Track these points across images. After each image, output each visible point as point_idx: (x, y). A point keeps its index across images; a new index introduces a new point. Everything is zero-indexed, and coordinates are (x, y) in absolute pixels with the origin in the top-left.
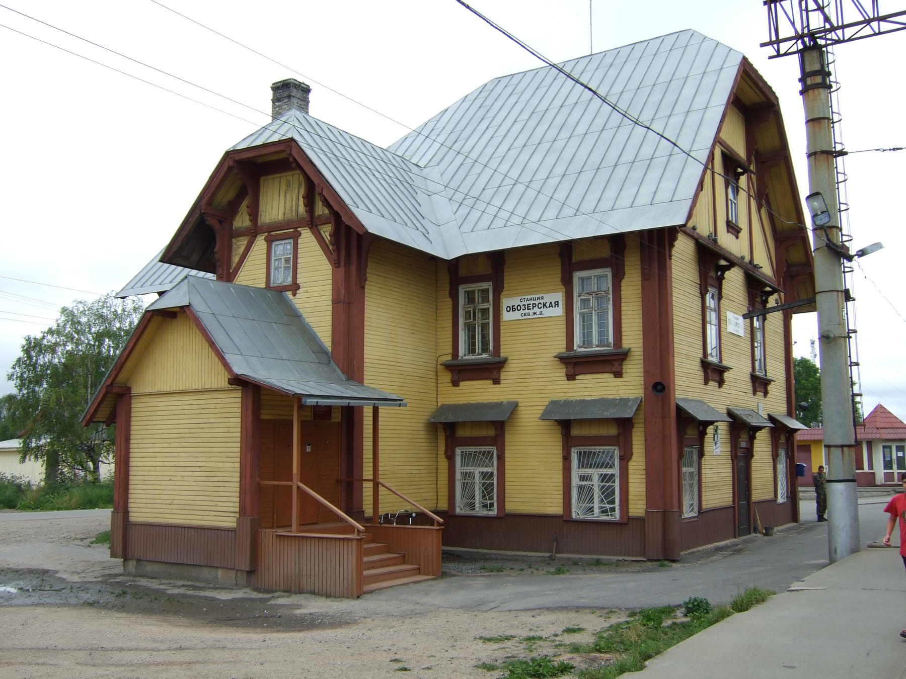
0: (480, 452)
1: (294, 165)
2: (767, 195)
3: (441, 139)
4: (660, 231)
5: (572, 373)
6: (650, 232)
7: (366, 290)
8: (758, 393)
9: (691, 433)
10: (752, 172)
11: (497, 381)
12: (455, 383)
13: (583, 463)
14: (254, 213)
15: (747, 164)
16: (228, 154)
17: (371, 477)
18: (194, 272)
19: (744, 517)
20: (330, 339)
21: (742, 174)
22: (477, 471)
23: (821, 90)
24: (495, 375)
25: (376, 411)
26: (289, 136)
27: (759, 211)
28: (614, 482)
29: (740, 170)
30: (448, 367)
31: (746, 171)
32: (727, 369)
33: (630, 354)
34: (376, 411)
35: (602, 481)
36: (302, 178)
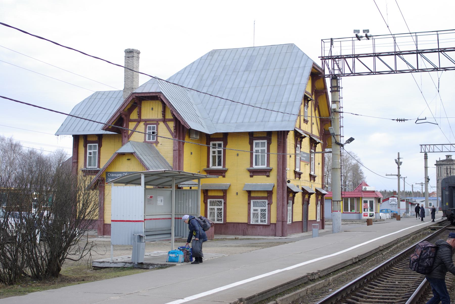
2: (318, 106)
4: (284, 132)
6: (281, 131)
9: (291, 195)
11: (224, 177)
14: (139, 114)
19: (304, 225)
21: (310, 100)
22: (216, 207)
23: (337, 92)
24: (223, 174)
30: (206, 171)
32: (302, 173)
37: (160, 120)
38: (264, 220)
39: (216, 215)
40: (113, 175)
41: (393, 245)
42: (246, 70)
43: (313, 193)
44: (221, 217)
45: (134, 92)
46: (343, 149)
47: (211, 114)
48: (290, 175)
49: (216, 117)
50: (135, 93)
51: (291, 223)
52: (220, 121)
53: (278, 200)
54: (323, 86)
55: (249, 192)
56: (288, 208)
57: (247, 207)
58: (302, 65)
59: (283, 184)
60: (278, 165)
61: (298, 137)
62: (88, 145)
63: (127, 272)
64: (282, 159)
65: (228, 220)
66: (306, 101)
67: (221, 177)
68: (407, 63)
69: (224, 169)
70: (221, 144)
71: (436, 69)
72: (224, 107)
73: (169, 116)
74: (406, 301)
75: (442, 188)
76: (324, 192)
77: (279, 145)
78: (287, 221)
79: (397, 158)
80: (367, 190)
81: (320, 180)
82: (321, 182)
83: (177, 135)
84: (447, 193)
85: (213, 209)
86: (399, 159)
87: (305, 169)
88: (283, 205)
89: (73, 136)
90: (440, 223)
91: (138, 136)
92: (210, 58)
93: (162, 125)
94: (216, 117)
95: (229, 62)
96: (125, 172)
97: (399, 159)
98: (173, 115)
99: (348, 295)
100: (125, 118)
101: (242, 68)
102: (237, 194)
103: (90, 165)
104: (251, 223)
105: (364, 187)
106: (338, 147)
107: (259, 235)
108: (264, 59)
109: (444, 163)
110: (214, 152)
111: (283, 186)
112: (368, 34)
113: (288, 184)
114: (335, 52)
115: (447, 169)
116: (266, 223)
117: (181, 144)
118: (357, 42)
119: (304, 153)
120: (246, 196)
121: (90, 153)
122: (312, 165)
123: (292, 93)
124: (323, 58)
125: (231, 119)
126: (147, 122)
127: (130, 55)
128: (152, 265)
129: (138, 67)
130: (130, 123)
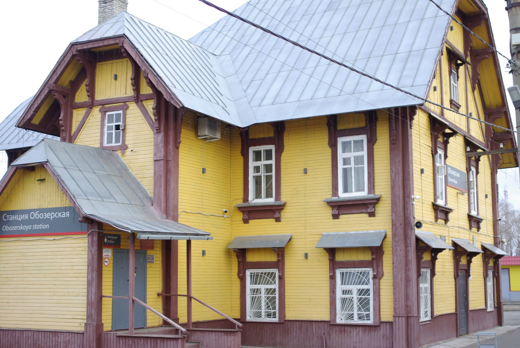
0: (265, 273)
1: (124, 55)
2: (479, 81)
3: (231, 34)
5: (337, 213)
6: (396, 109)
7: (180, 150)
8: (473, 229)
9: (427, 257)
10: (468, 63)
11: (278, 220)
12: (246, 221)
13: (345, 282)
15: (464, 57)
16: (73, 45)
17: (186, 293)
18: (50, 137)
20: (152, 187)
21: (461, 65)
22: (263, 287)
25: (189, 242)
26: (120, 33)
27: (473, 92)
28: (369, 295)
29: (459, 62)
30: (241, 209)
31: (464, 62)
33: (381, 199)
34: (189, 242)
35: (360, 295)
36: (129, 62)
38: (365, 313)
39: (263, 304)
43: (478, 253)
44: (274, 308)
47: (251, 91)
48: (421, 211)
49: (260, 94)
51: (429, 318)
55: (332, 252)
56: (421, 285)
57: (328, 285)
59: (405, 231)
60: (393, 188)
61: (439, 130)
64: (401, 174)
65: (290, 315)
66: (453, 66)
67: (272, 221)
70: (270, 151)
72: (278, 75)
76: (498, 251)
77: (393, 143)
78: (419, 317)
82: (491, 233)
83: (162, 128)
88: (407, 280)
93: (133, 108)
94: (260, 94)
96: (35, 210)
100: (62, 101)
101: (320, 7)
102: (306, 256)
104: (338, 321)
110: (257, 169)
111: (406, 237)
113: (418, 232)
116: (370, 322)
117: (171, 147)
120: (325, 259)
122: (472, 195)
123: (420, 34)
126: (106, 106)
130: (75, 112)
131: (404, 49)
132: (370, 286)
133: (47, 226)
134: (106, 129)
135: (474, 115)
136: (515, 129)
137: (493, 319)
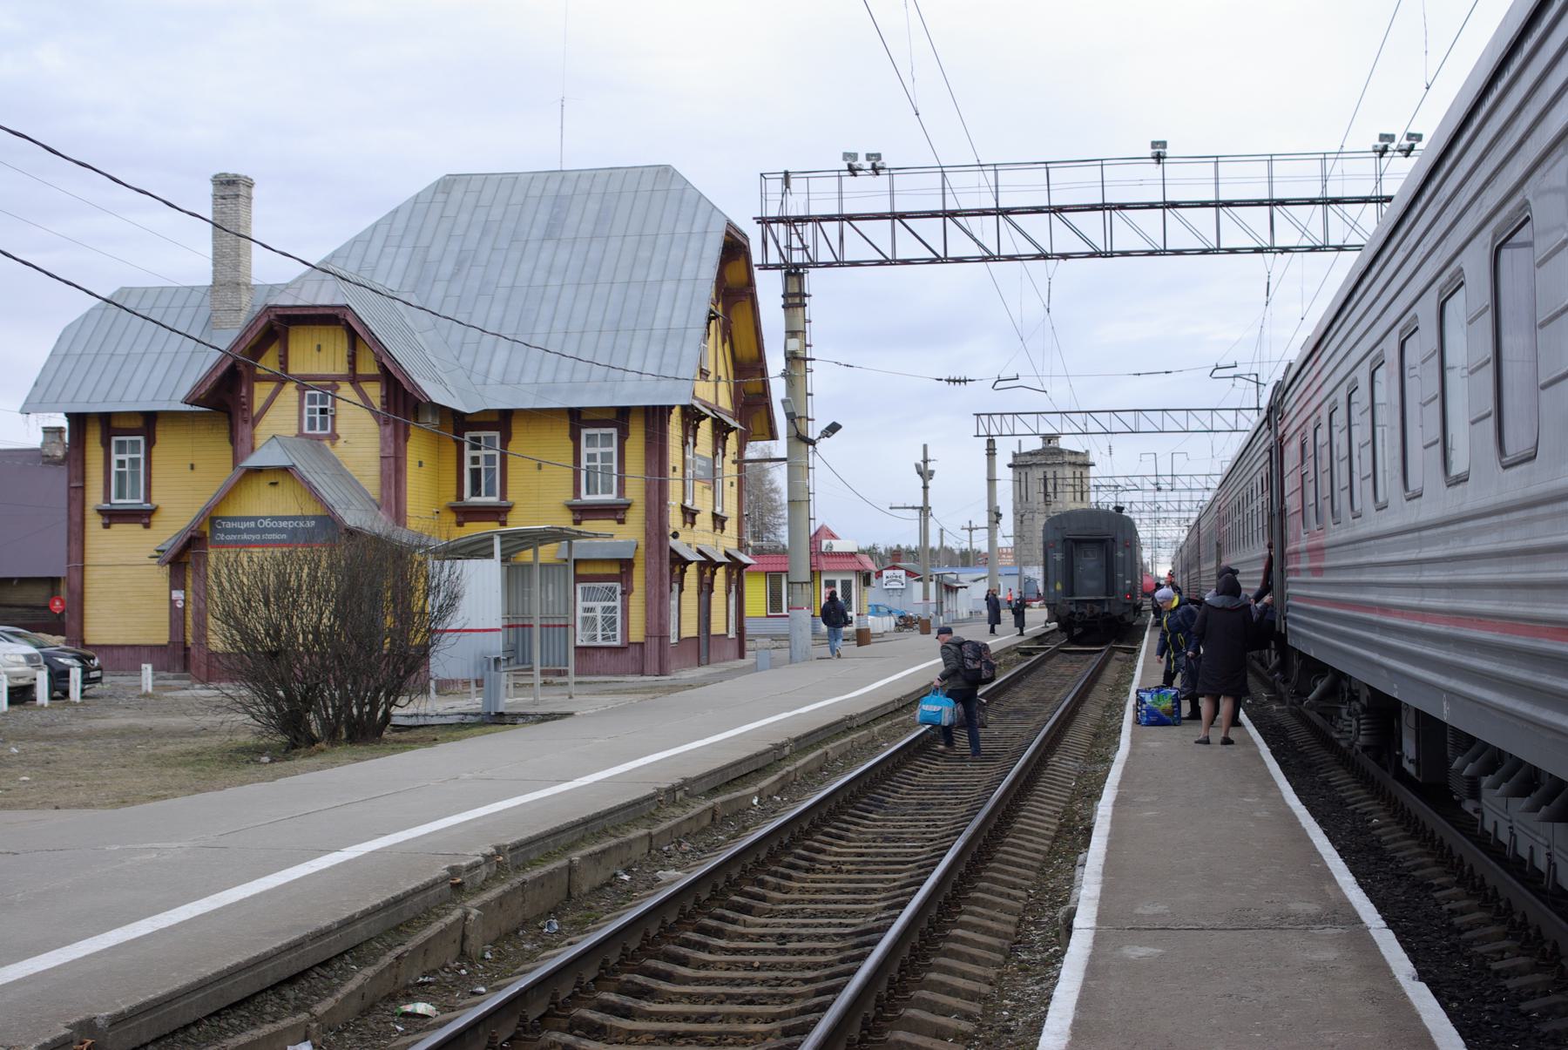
4: (662, 408)
19: (703, 647)
22: (598, 606)
30: (454, 509)
37: (341, 378)
40: (230, 525)
41: (356, 952)
42: (548, 235)
45: (272, 303)
46: (815, 451)
48: (675, 520)
50: (275, 307)
52: (489, 381)
53: (647, 582)
54: (744, 278)
58: (697, 228)
60: (647, 492)
62: (114, 439)
63: (475, 730)
67: (139, 527)
68: (979, 244)
69: (504, 503)
71: (1043, 256)
73: (367, 366)
74: (806, 1030)
75: (1045, 544)
76: (745, 559)
79: (919, 459)
80: (835, 549)
81: (735, 527)
82: (735, 534)
84: (1058, 557)
85: (590, 610)
86: (926, 461)
87: (704, 501)
89: (67, 415)
90: (1039, 638)
91: (279, 422)
92: (440, 197)
94: (481, 366)
95: (496, 213)
96: (265, 518)
97: (926, 461)
98: (383, 367)
99: (701, 907)
103: (121, 495)
105: (825, 542)
106: (803, 445)
107: (598, 674)
108: (593, 206)
109: (1035, 460)
111: (661, 547)
112: (878, 164)
114: (795, 208)
115: (1045, 479)
116: (618, 643)
117: (401, 441)
118: (848, 181)
119: (701, 457)
121: (121, 463)
123: (678, 304)
124: (764, 221)
125: (522, 371)
126: (303, 383)
127: (229, 191)
128: (522, 715)
129: (248, 226)
130: (257, 386)
131: (659, 324)
132: (618, 603)
133: (284, 536)
134: (306, 412)
135: (723, 378)
136: (775, 778)
137: (732, 649)
